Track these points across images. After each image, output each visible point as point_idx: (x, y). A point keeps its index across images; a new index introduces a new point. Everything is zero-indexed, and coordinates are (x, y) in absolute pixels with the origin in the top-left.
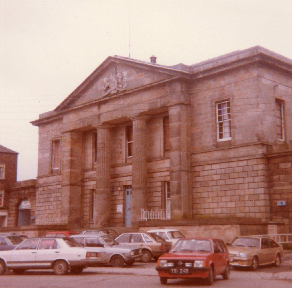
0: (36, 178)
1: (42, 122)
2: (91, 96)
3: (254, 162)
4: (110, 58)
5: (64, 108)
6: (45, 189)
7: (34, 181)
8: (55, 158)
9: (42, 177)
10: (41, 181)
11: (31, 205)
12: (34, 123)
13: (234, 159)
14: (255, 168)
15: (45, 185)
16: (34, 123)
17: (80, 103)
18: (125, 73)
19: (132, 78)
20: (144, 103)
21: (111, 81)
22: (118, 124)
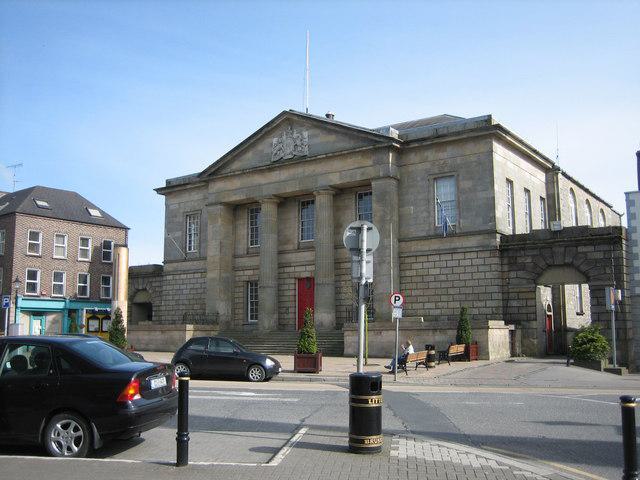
0: (159, 261)
1: (171, 189)
2: (249, 159)
3: (487, 254)
4: (284, 113)
5: (213, 174)
6: (177, 277)
7: (156, 266)
8: (453, 251)
9: (171, 262)
10: (168, 268)
11: (13, 214)
12: (159, 191)
13: (459, 250)
14: (488, 261)
15: (174, 273)
16: (159, 191)
17: (236, 165)
18: (306, 134)
19: (317, 141)
20: (338, 173)
21: (284, 145)
22: (285, 198)
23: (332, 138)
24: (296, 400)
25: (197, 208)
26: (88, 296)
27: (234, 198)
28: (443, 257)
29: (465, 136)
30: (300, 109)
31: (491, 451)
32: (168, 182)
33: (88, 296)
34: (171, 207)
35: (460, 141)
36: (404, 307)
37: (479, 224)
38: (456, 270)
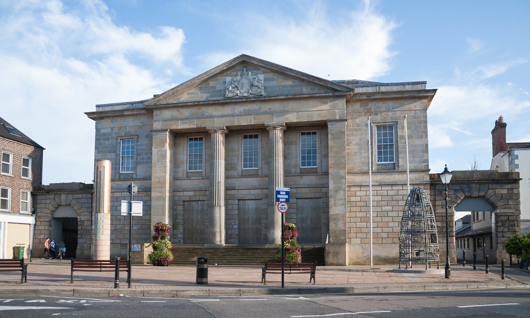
1: (99, 115)
12: (89, 114)
18: (261, 77)
21: (242, 85)
23: (289, 83)
24: (55, 314)
25: (134, 133)
26: (121, 172)
27: (180, 126)
28: (384, 188)
29: (406, 95)
30: (245, 54)
31: (520, 290)
32: (155, 96)
33: (121, 172)
34: (102, 131)
35: (401, 98)
36: (292, 228)
37: (422, 166)
38: (395, 198)
